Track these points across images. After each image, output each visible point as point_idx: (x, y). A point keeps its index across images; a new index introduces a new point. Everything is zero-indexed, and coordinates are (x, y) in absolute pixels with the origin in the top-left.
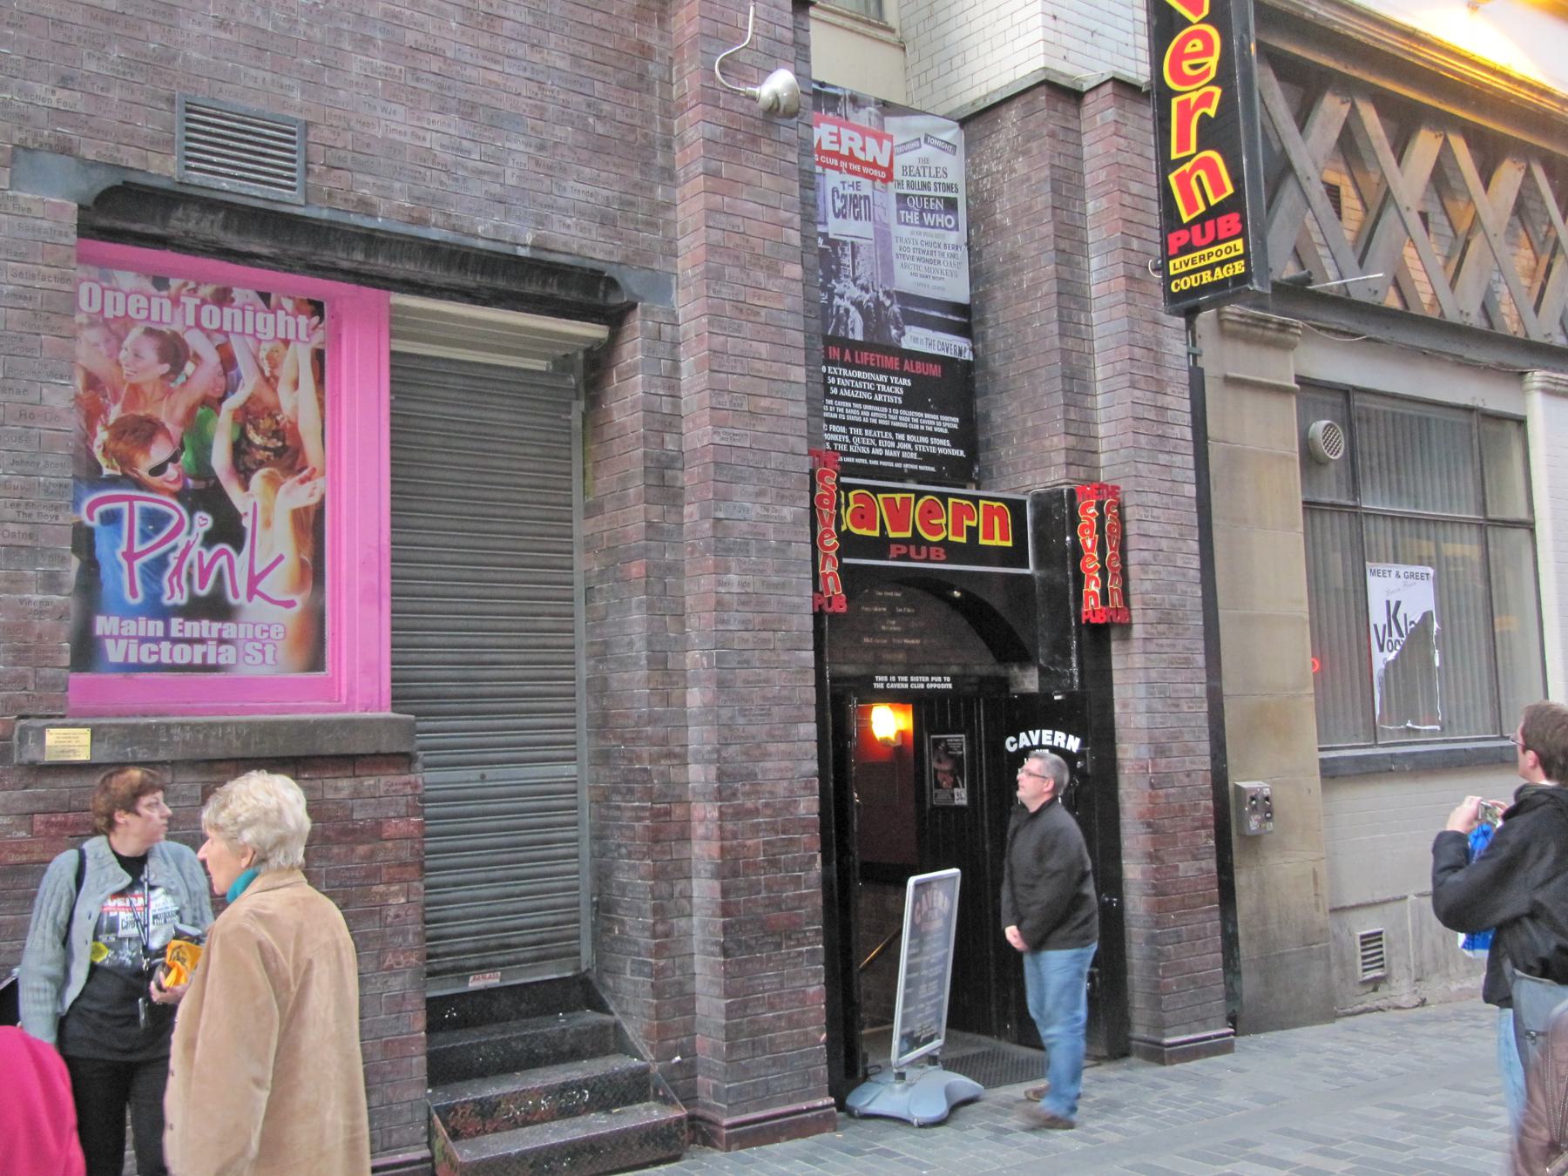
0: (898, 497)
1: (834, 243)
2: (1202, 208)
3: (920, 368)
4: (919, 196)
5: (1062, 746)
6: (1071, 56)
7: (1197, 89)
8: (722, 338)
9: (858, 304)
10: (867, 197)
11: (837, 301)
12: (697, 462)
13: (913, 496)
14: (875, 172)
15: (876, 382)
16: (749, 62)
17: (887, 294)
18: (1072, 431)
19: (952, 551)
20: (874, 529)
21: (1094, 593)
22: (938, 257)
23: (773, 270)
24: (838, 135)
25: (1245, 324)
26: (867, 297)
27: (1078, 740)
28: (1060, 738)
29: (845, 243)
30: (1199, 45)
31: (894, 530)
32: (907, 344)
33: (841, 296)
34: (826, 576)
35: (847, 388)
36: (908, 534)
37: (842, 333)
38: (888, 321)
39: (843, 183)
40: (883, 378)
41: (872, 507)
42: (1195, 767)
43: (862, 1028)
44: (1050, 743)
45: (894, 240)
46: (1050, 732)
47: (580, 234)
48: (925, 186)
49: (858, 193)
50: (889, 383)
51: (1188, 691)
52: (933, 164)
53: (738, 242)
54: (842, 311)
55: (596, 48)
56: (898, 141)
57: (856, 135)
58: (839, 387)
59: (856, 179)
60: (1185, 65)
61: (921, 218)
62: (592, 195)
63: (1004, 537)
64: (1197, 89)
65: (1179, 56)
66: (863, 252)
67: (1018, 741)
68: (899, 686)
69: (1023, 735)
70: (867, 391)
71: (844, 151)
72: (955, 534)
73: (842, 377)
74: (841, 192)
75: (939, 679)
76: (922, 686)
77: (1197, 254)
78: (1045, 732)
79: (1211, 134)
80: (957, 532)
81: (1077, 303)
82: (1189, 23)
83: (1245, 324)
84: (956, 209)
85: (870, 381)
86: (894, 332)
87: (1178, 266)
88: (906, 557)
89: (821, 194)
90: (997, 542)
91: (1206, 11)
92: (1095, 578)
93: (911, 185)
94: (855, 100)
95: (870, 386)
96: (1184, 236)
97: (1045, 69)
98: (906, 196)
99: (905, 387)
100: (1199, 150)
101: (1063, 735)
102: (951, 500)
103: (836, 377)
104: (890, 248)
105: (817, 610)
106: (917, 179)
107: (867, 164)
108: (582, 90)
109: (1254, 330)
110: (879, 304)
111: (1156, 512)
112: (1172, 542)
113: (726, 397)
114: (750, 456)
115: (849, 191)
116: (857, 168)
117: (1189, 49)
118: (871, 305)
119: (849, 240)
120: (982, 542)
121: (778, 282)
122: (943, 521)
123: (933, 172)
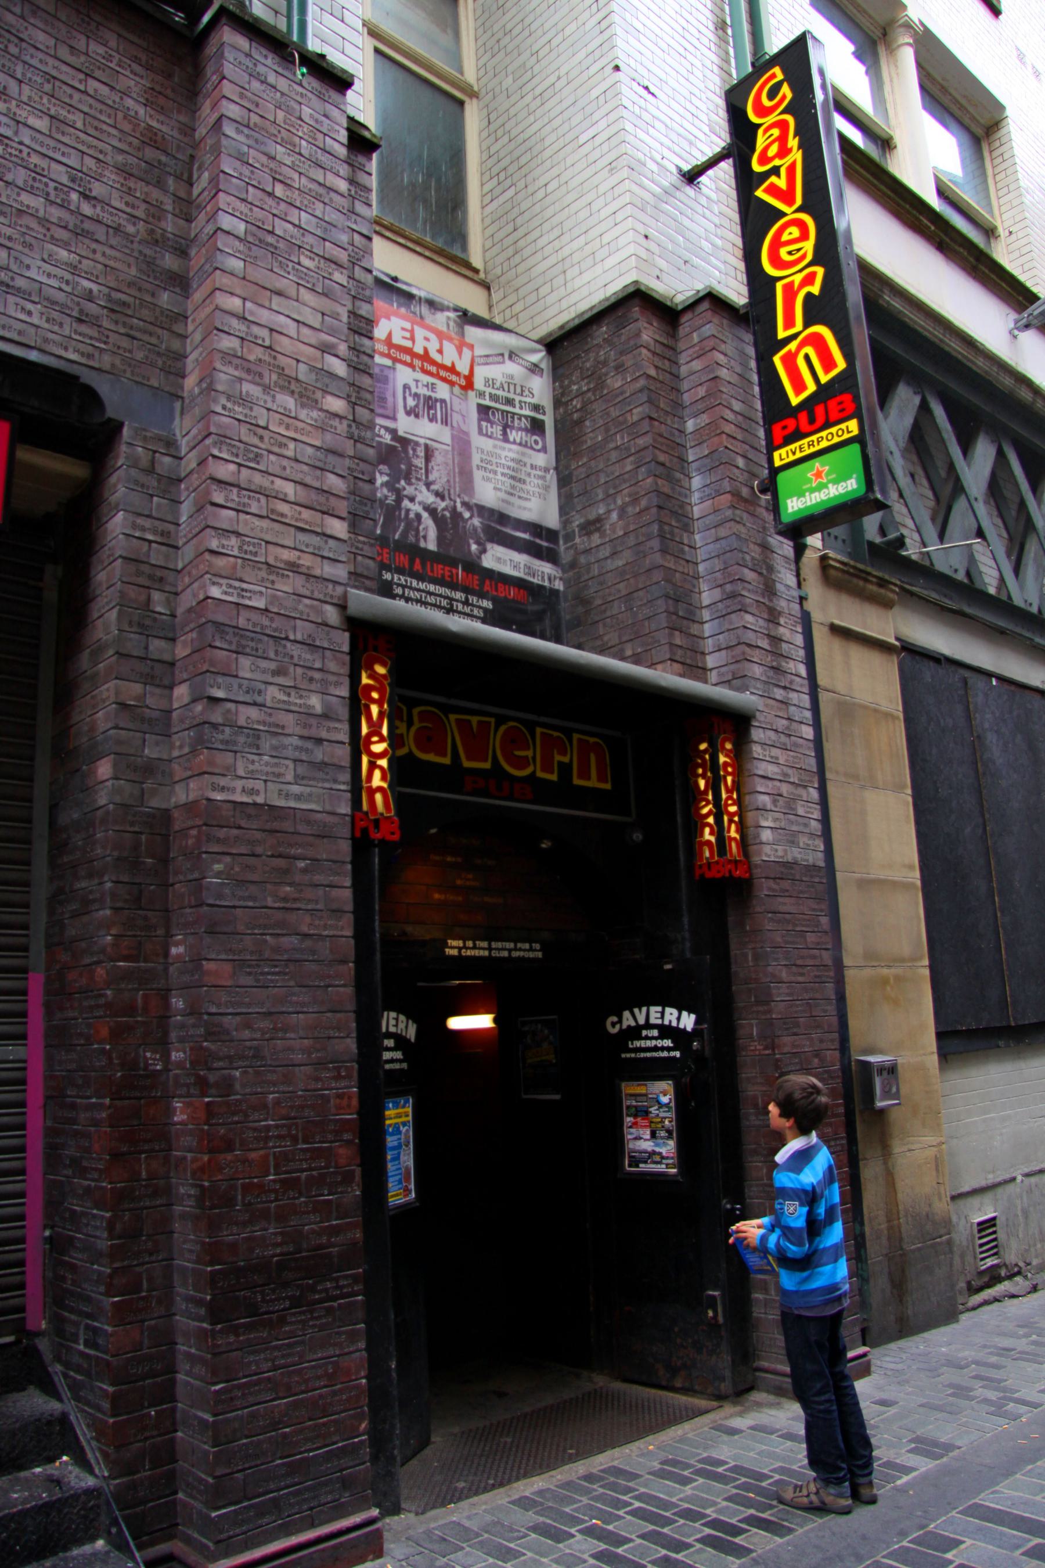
0: (475, 720)
1: (404, 442)
2: (811, 387)
4: (503, 411)
5: (674, 1024)
6: (664, 276)
7: (800, 271)
8: (232, 467)
9: (432, 511)
10: (443, 401)
11: (406, 503)
12: (192, 626)
13: (493, 720)
14: (454, 378)
15: (451, 599)
16: (289, 163)
17: (465, 504)
18: (677, 658)
19: (536, 788)
21: (709, 842)
22: (523, 477)
23: (306, 397)
24: (412, 332)
25: (847, 573)
26: (443, 505)
27: (693, 1017)
28: (671, 1015)
29: (417, 444)
30: (794, 232)
31: (469, 758)
32: (488, 562)
33: (412, 500)
34: (372, 792)
36: (487, 765)
37: (412, 539)
39: (417, 381)
40: (459, 595)
42: (824, 1046)
44: (659, 1022)
45: (474, 451)
46: (659, 1009)
47: (46, 326)
48: (509, 402)
49: (433, 395)
50: (466, 603)
51: (814, 957)
54: (412, 515)
55: (88, 119)
56: (478, 352)
57: (432, 336)
59: (431, 380)
60: (783, 252)
61: (505, 434)
62: (67, 283)
63: (601, 778)
64: (800, 271)
65: (776, 244)
66: (438, 459)
67: (620, 1021)
69: (626, 1014)
71: (419, 349)
72: (544, 769)
73: (411, 588)
74: (414, 390)
75: (527, 946)
76: (505, 954)
77: (805, 441)
79: (814, 311)
80: (547, 767)
81: (678, 521)
82: (784, 215)
83: (847, 573)
85: (446, 597)
86: (474, 547)
87: (784, 456)
89: (390, 386)
90: (593, 783)
91: (799, 201)
92: (709, 825)
93: (494, 398)
94: (433, 305)
96: (791, 423)
97: (636, 282)
98: (488, 408)
99: (485, 610)
100: (806, 325)
101: (675, 1012)
102: (539, 730)
103: (404, 587)
105: (358, 834)
106: (500, 393)
108: (64, 160)
109: (855, 581)
110: (456, 515)
111: (775, 752)
112: (791, 788)
113: (233, 541)
114: (266, 622)
115: (423, 391)
117: (785, 237)
118: (448, 514)
119: (422, 441)
120: (577, 781)
121: (315, 414)
123: (518, 390)
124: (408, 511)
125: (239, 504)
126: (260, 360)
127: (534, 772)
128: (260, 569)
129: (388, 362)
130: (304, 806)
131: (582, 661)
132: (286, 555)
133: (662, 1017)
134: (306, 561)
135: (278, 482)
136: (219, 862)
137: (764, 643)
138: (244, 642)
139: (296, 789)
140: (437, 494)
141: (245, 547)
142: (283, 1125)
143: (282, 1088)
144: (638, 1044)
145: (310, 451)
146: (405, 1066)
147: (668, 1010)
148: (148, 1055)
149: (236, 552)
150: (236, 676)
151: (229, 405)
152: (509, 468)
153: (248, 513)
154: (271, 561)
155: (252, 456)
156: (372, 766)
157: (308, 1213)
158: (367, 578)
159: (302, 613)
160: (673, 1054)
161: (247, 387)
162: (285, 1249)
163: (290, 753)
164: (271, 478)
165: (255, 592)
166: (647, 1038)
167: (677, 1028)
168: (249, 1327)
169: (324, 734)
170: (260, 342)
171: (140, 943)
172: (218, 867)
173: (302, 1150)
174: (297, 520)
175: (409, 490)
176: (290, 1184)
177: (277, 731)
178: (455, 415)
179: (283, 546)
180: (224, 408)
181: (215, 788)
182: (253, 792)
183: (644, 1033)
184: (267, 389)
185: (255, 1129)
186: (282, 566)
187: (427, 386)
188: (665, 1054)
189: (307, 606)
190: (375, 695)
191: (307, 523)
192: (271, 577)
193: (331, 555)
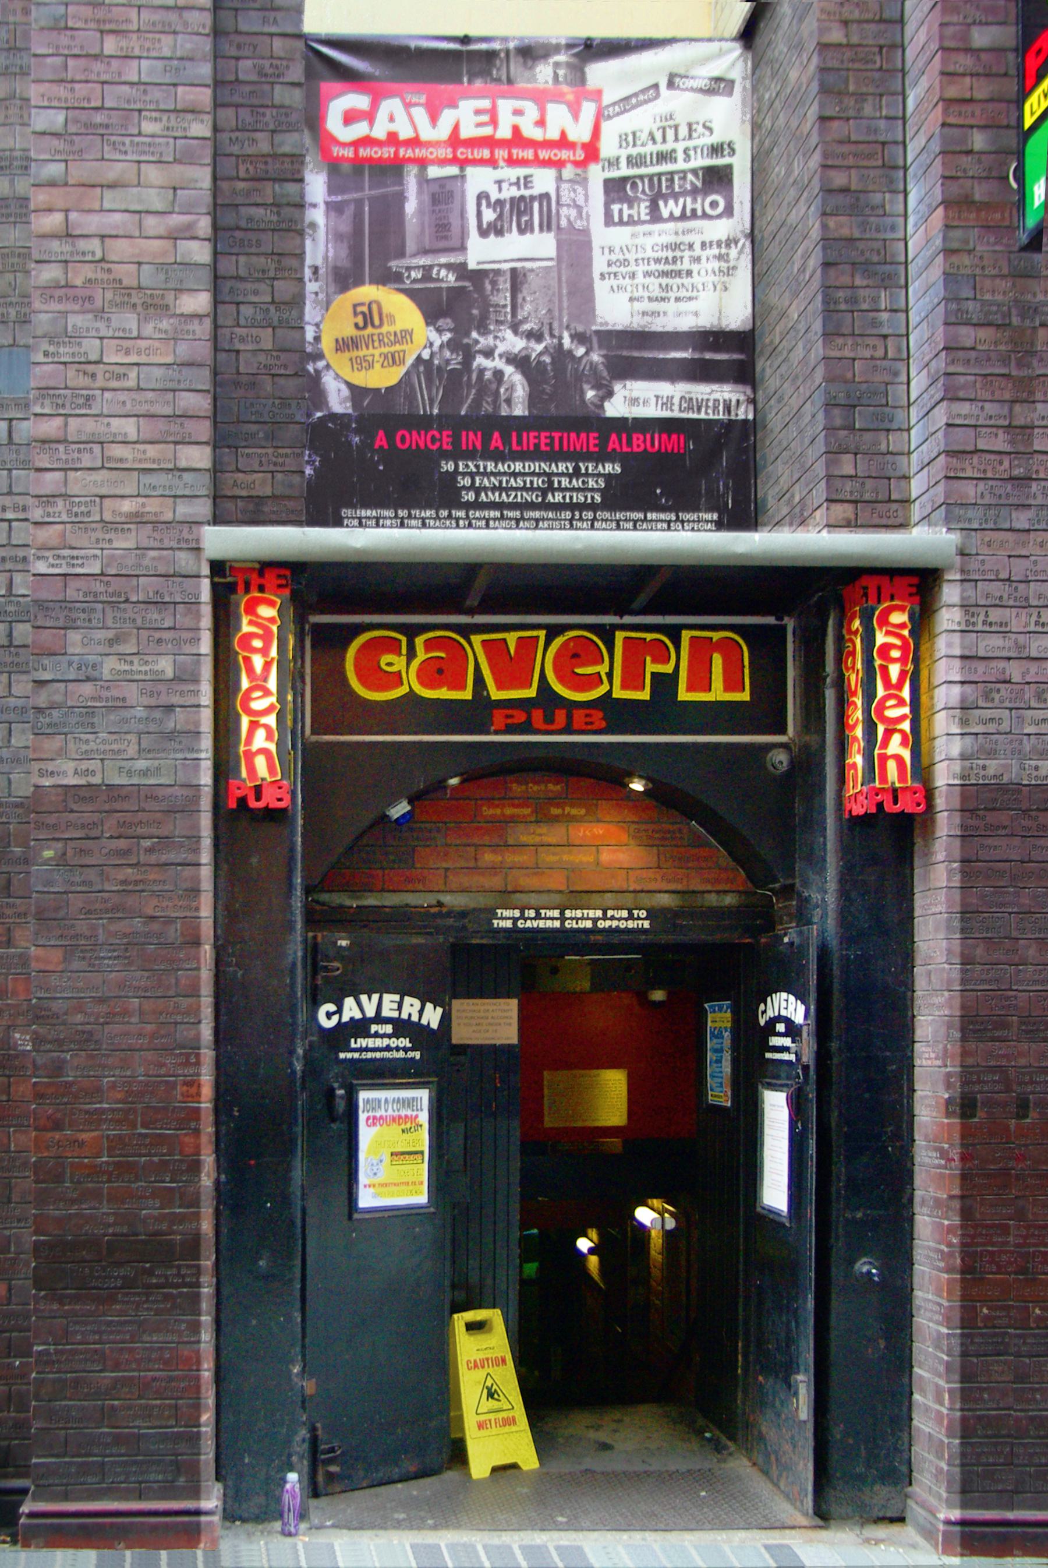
0: (512, 639)
1: (478, 276)
3: (639, 444)
5: (415, 1018)
8: (58, 422)
9: (520, 362)
10: (546, 196)
11: (480, 361)
15: (549, 475)
20: (462, 687)
21: (899, 759)
26: (539, 348)
28: (411, 1007)
29: (498, 272)
31: (500, 686)
32: (615, 408)
33: (489, 353)
35: (494, 489)
36: (531, 693)
37: (487, 408)
38: (579, 378)
39: (499, 182)
41: (458, 655)
43: (798, 1373)
44: (395, 1014)
45: (596, 253)
46: (397, 997)
49: (527, 193)
52: (682, 121)
53: (91, 275)
54: (488, 375)
56: (607, 99)
58: (478, 491)
63: (732, 683)
67: (339, 1011)
68: (542, 924)
69: (349, 1002)
70: (532, 489)
73: (486, 474)
74: (494, 196)
75: (625, 914)
76: (589, 924)
78: (387, 998)
84: (730, 181)
86: (590, 394)
88: (526, 728)
90: (718, 693)
95: (538, 482)
98: (624, 180)
99: (608, 477)
101: (417, 1003)
103: (472, 475)
104: (588, 264)
107: (548, 144)
110: (560, 354)
116: (529, 154)
118: (547, 359)
120: (684, 695)
122: (603, 669)
123: (683, 131)
124: (482, 371)
125: (67, 461)
126: (90, 280)
127: (610, 692)
128: (94, 530)
129: (453, 170)
130: (152, 781)
131: (579, 546)
132: (127, 506)
133: (400, 1008)
134: (152, 506)
135: (115, 422)
136: (49, 848)
137: (1001, 442)
138: (74, 615)
139: (142, 764)
140: (530, 335)
141: (75, 509)
142: (119, 1110)
143: (117, 1072)
144: (363, 1042)
145: (158, 372)
146: (417, 1055)
147: (408, 1000)
148: (17, 1036)
149: (64, 517)
150: (65, 654)
151: (52, 349)
152: (658, 261)
153: (76, 470)
154: (107, 517)
155: (81, 401)
156: (254, 725)
157: (146, 1198)
158: (289, 498)
159: (147, 567)
160: (411, 1054)
161: (74, 320)
162: (118, 1229)
163: (134, 726)
164: (106, 420)
165: (87, 557)
166: (376, 1035)
167: (418, 1024)
168: (76, 1299)
169: (175, 700)
170: (89, 258)
171: (9, 929)
172: (48, 854)
173: (140, 1134)
174: (140, 461)
175: (485, 341)
176: (124, 1169)
177: (121, 705)
178: (564, 211)
179: (122, 497)
180: (46, 354)
181: (42, 773)
182: (87, 772)
183: (374, 1028)
184: (100, 313)
185: (87, 1112)
186: (123, 519)
187: (517, 184)
188: (401, 1054)
189: (154, 558)
190: (257, 643)
191: (154, 461)
192: (107, 537)
193: (187, 492)
